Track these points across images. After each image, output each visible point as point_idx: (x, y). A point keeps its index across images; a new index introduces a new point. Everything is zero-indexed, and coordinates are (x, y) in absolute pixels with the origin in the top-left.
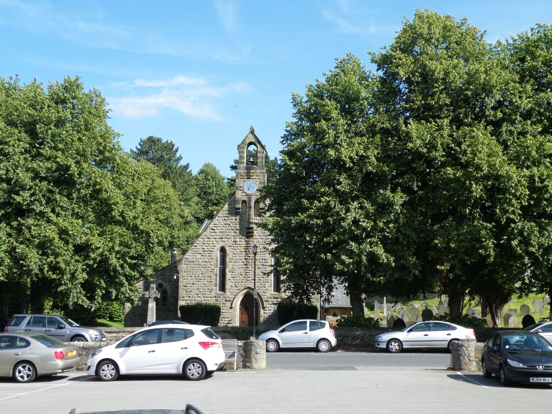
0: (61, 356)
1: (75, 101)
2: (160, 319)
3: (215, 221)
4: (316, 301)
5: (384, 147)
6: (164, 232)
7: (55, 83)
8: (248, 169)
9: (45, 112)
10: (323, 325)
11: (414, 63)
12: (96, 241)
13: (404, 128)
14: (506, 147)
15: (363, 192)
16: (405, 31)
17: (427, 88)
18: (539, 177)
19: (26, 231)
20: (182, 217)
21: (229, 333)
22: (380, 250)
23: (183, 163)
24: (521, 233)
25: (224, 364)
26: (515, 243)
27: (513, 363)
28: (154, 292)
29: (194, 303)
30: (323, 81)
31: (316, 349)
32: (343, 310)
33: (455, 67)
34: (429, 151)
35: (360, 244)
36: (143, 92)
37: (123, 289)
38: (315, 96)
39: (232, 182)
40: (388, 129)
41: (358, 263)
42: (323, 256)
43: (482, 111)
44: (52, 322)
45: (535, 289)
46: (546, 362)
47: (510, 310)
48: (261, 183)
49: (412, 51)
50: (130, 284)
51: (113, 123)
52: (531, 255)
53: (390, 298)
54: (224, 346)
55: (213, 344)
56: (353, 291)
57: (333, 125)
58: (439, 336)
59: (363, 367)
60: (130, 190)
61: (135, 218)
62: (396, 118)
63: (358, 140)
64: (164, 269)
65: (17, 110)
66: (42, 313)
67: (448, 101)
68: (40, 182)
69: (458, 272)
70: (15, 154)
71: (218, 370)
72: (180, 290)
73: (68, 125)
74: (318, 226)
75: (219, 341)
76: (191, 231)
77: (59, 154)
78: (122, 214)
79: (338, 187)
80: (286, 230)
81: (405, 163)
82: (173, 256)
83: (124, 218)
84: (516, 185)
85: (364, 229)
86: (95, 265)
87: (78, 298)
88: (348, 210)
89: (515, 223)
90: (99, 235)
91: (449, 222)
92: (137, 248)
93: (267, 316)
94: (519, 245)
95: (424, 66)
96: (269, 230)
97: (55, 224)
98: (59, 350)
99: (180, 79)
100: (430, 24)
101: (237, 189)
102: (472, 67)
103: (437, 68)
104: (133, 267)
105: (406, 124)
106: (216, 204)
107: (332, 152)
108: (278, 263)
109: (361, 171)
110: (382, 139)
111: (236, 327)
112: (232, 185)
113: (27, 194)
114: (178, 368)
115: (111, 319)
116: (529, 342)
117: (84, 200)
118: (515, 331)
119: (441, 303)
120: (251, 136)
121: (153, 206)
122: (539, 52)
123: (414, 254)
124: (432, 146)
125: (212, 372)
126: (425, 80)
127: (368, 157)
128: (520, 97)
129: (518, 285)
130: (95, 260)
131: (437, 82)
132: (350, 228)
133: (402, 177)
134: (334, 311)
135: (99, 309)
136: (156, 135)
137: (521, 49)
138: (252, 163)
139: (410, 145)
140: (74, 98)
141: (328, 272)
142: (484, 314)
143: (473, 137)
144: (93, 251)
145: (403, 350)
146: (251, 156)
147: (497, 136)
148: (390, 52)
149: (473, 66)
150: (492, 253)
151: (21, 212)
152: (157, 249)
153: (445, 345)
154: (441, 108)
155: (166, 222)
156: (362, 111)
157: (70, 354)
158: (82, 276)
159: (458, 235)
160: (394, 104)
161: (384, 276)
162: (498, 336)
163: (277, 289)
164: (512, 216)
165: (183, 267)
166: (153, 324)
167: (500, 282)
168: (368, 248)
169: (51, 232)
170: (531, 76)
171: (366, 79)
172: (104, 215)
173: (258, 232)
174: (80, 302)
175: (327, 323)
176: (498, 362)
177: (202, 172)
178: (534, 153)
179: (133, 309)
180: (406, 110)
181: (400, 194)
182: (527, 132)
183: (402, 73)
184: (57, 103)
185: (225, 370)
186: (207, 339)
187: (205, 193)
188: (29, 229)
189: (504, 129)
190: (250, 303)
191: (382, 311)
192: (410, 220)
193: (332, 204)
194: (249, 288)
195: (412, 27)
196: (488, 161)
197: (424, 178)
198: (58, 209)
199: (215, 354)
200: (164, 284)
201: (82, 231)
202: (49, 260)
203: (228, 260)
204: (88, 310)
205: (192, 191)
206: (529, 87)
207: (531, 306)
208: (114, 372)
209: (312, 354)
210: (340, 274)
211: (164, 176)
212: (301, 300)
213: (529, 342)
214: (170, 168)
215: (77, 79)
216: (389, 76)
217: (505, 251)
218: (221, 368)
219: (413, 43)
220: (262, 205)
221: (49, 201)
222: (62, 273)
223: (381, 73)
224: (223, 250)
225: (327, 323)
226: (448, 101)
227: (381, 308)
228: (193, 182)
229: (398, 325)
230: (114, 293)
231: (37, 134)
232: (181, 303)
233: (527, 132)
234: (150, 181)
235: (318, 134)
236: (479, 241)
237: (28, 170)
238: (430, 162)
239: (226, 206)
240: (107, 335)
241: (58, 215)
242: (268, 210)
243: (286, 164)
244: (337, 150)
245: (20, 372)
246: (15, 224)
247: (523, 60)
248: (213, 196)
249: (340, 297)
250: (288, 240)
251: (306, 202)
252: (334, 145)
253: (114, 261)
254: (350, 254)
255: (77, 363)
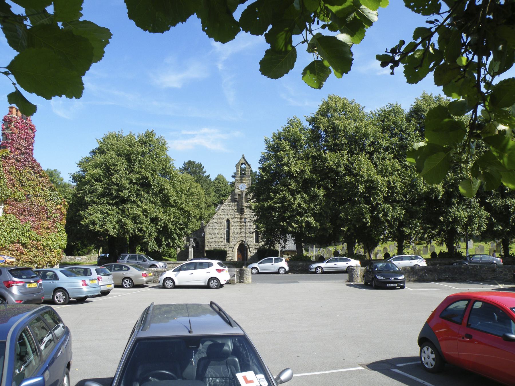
0: (145, 275)
1: (151, 143)
2: (195, 257)
3: (224, 205)
4: (278, 247)
5: (314, 165)
6: (197, 211)
7: (141, 134)
8: (241, 177)
9: (135, 149)
10: (281, 260)
11: (328, 122)
12: (161, 216)
13: (323, 155)
14: (376, 166)
15: (303, 189)
16: (323, 105)
17: (335, 135)
18: (393, 182)
19: (126, 211)
20: (206, 203)
21: (231, 264)
22: (312, 220)
23: (206, 174)
24: (383, 210)
25: (229, 280)
26: (380, 215)
27: (379, 277)
28: (192, 243)
29: (213, 248)
30: (281, 130)
31: (278, 273)
32: (292, 252)
33: (349, 124)
34: (337, 168)
35: (301, 217)
36: (186, 137)
37: (175, 241)
38: (277, 138)
39: (233, 184)
40: (315, 156)
41: (301, 227)
42: (282, 223)
43: (364, 147)
44: (140, 258)
45: (390, 239)
46: (395, 276)
47: (378, 250)
48: (248, 185)
49: (327, 115)
50: (179, 239)
51: (170, 153)
52: (388, 221)
53: (318, 246)
54: (229, 271)
55: (223, 270)
56: (297, 242)
57: (287, 154)
58: (342, 265)
59: (302, 282)
60: (179, 189)
61: (182, 204)
62: (319, 150)
63: (300, 161)
64: (197, 230)
65: (122, 148)
66: (135, 253)
67: (346, 142)
68: (133, 185)
69: (352, 231)
70: (121, 170)
71: (226, 283)
72: (206, 241)
73: (147, 155)
74: (279, 207)
75: (227, 268)
76: (211, 211)
77: (143, 170)
78: (174, 201)
79: (290, 187)
80: (261, 210)
81: (324, 174)
82: (202, 224)
83: (176, 203)
84: (381, 186)
85: (304, 209)
86: (161, 229)
87: (153, 246)
88: (295, 199)
89: (380, 205)
90: (163, 213)
91: (348, 205)
92: (183, 219)
93: (252, 255)
94: (382, 216)
95: (333, 124)
96: (253, 210)
97: (141, 207)
98: (144, 272)
99: (205, 130)
100: (336, 102)
101: (235, 188)
102: (358, 124)
103: (341, 124)
104: (181, 229)
105: (325, 153)
106: (224, 196)
107: (286, 168)
108: (257, 227)
109: (301, 178)
110: (312, 161)
111: (236, 261)
112: (233, 186)
113: (126, 192)
114: (205, 282)
115: (170, 257)
116: (387, 267)
117: (156, 194)
118: (380, 261)
119: (343, 247)
120: (243, 159)
121: (191, 197)
122: (391, 117)
123: (330, 222)
124: (338, 165)
125: (223, 284)
126: (334, 130)
127: (305, 171)
128: (382, 140)
129: (382, 237)
130: (161, 226)
131: (340, 131)
132: (296, 208)
133: (323, 181)
134: (287, 253)
135: (163, 252)
136: (192, 160)
137: (382, 116)
138: (244, 174)
139: (327, 164)
140: (151, 141)
141: (285, 232)
142: (365, 253)
143: (359, 160)
144: (160, 221)
145: (323, 272)
146: (243, 170)
147: (371, 160)
148: (316, 116)
149: (359, 124)
150: (369, 221)
151: (124, 201)
152: (194, 220)
153: (345, 269)
154: (343, 145)
155: (198, 206)
156: (302, 146)
157: (149, 275)
158: (155, 235)
159: (352, 212)
160: (318, 143)
161: (314, 233)
162: (372, 264)
163: (257, 241)
164: (379, 202)
165: (207, 230)
166: (192, 260)
167: (373, 236)
168: (306, 219)
169: (139, 211)
170: (388, 129)
171: (304, 129)
172: (166, 202)
173: (247, 211)
174: (154, 248)
175: (284, 259)
176: (371, 277)
177: (216, 179)
178: (390, 169)
179: (181, 251)
180: (325, 146)
181: (322, 190)
182: (386, 158)
183: (322, 127)
184: (141, 144)
185: (230, 284)
186: (220, 268)
187: (218, 190)
188: (128, 210)
189: (375, 156)
190: (243, 249)
191: (313, 252)
192: (327, 203)
193: (287, 195)
194: (242, 241)
195: (327, 103)
196: (367, 173)
197: (334, 181)
198: (142, 199)
199: (224, 276)
200: (197, 239)
201: (155, 211)
202: (138, 226)
203: (231, 226)
204: (158, 252)
205: (212, 189)
206: (386, 135)
207: (388, 248)
208: (172, 284)
209: (276, 275)
210: (291, 233)
211: (197, 181)
212: (270, 247)
213: (387, 267)
214: (200, 177)
215: (153, 131)
216: (315, 128)
217: (375, 220)
218: (228, 283)
219: (328, 111)
220: (248, 197)
221: (137, 195)
222: (145, 232)
223: (311, 127)
224: (228, 221)
225: (284, 259)
226: (346, 142)
227: (312, 251)
228: (212, 184)
229: (321, 259)
230: (172, 244)
231: (131, 160)
232: (206, 249)
233: (386, 158)
234: (189, 184)
235: (279, 158)
236: (363, 215)
237: (127, 179)
238: (337, 173)
239: (230, 197)
240: (168, 265)
241: (142, 202)
242: (252, 199)
243: (261, 174)
244: (289, 167)
245: (125, 283)
246: (121, 207)
247: (383, 121)
248: (222, 192)
249: (291, 245)
250: (263, 215)
251: (272, 195)
252: (288, 164)
253: (170, 226)
254: (296, 222)
255: (153, 279)
